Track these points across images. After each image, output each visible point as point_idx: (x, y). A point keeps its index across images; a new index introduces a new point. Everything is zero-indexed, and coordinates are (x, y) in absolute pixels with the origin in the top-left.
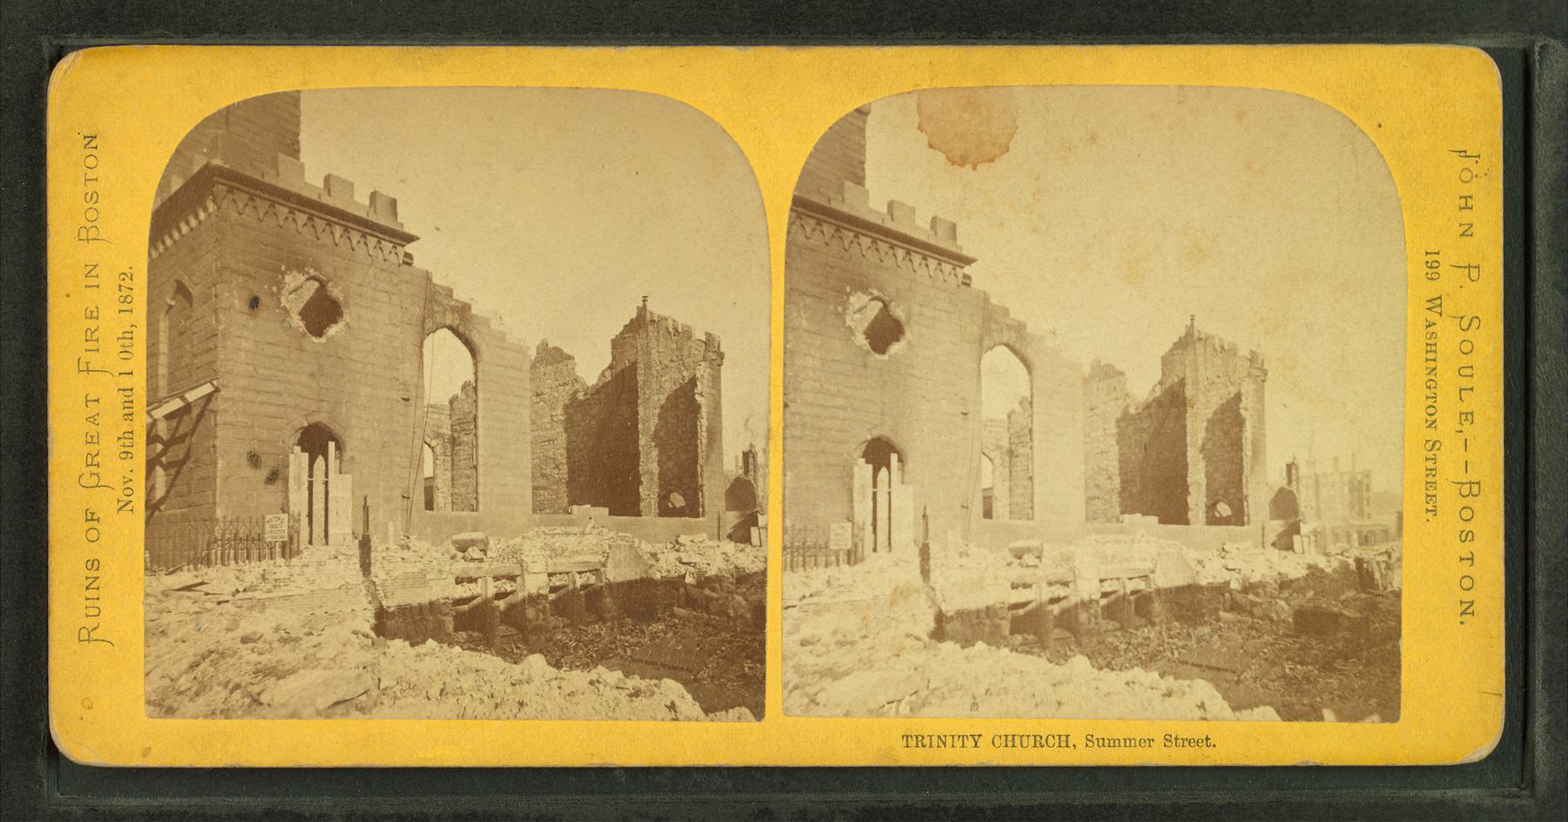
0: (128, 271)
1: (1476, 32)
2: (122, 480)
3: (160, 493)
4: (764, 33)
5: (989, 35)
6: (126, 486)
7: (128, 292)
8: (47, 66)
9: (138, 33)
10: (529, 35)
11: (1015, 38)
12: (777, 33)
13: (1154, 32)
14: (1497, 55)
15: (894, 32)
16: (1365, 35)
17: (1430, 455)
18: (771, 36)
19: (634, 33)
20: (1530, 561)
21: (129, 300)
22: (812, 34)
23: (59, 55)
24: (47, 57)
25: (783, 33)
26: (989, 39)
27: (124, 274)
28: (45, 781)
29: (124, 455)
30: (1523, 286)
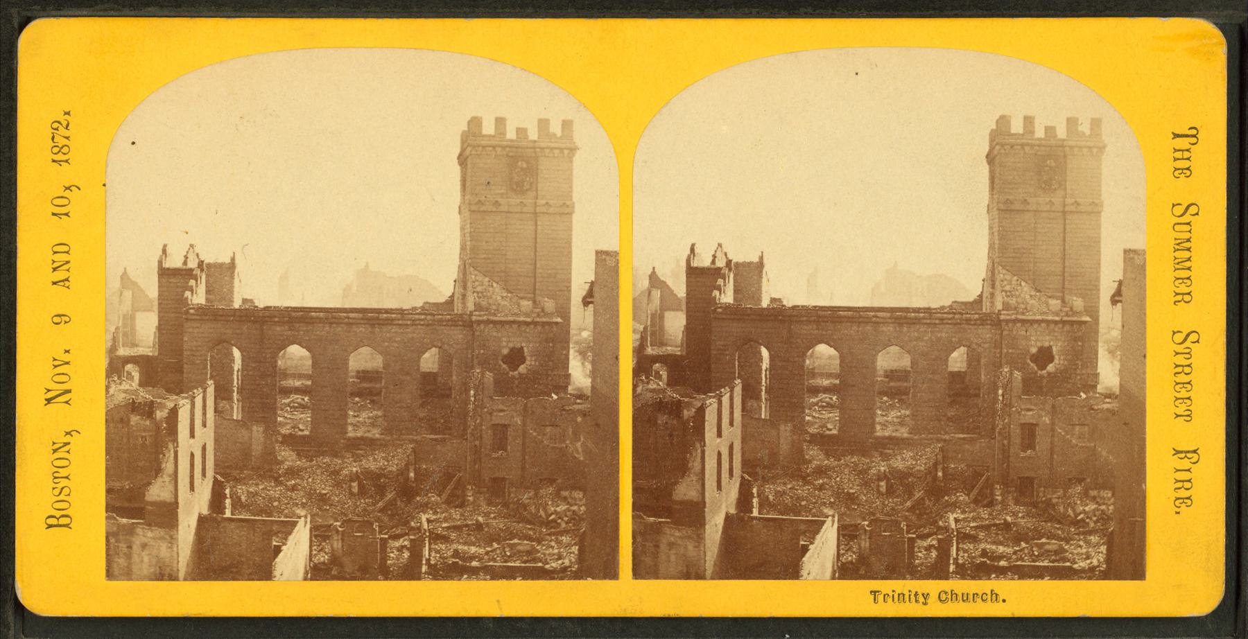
5: (797, 12)
10: (415, 9)
12: (621, 9)
22: (650, 10)
28: (12, 625)
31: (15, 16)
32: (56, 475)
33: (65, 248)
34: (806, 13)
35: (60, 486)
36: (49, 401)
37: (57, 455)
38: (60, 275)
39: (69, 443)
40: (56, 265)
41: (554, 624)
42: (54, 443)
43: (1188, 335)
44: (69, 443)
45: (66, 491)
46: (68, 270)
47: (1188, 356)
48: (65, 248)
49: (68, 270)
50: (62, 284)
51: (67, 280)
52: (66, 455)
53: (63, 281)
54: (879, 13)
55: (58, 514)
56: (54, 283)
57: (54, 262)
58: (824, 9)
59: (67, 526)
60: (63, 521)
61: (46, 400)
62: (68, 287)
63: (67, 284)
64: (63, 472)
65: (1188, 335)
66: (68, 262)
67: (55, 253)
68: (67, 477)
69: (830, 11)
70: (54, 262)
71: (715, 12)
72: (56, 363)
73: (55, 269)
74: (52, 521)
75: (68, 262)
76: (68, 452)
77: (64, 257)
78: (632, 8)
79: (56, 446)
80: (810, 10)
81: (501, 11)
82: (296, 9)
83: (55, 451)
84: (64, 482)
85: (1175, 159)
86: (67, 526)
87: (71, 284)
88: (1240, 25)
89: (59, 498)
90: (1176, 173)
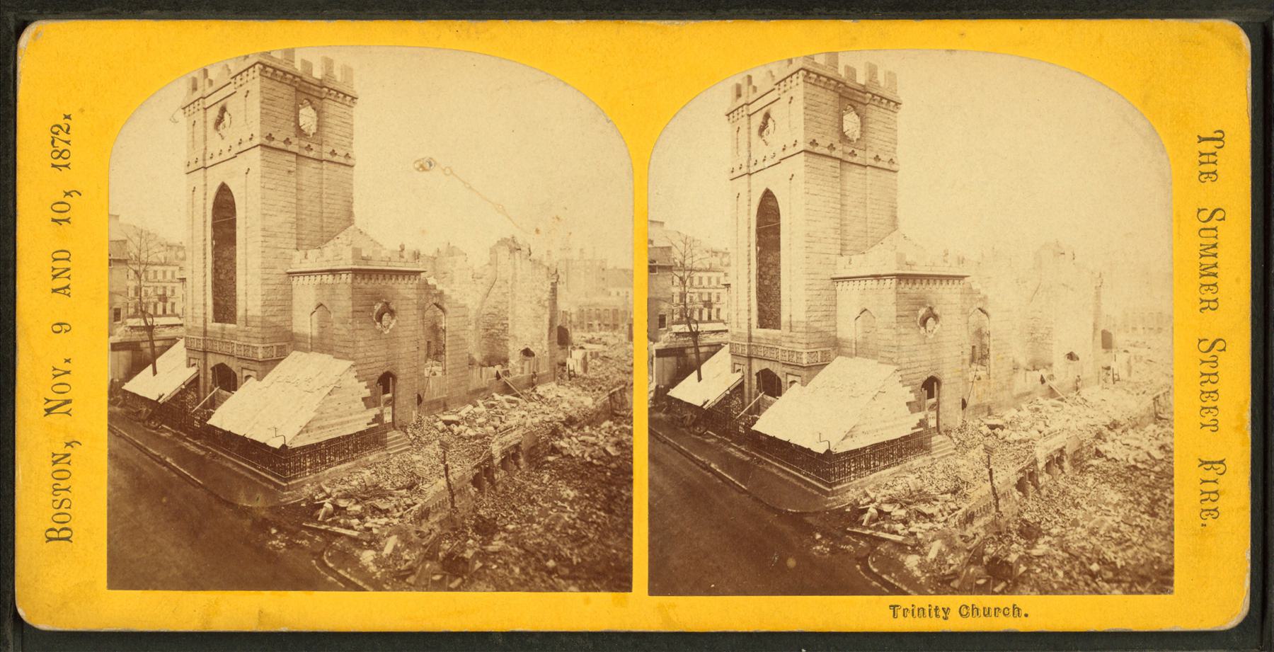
0: (62, 122)
1: (1223, 9)
2: (51, 373)
3: (570, 444)
4: (620, 9)
5: (811, 12)
6: (58, 380)
7: (66, 146)
8: (13, 38)
9: (90, 10)
10: (421, 11)
11: (833, 14)
13: (951, 9)
14: (1246, 28)
15: (731, 8)
16: (1128, 11)
17: (1207, 357)
18: (626, 12)
19: (509, 10)
20: (1262, 445)
21: (65, 154)
24: (13, 29)
25: (636, 10)
26: (812, 14)
27: (60, 127)
29: (57, 328)
30: (1262, 223)
31: (12, 19)
33: (65, 255)
34: (819, 14)
35: (60, 499)
36: (49, 411)
37: (57, 466)
40: (56, 272)
43: (1214, 212)
45: (66, 504)
46: (68, 278)
48: (65, 255)
49: (68, 278)
50: (62, 291)
51: (67, 287)
53: (64, 288)
54: (894, 13)
55: (58, 527)
56: (54, 291)
57: (54, 269)
59: (67, 539)
60: (64, 534)
62: (68, 295)
64: (63, 484)
65: (1214, 212)
66: (68, 269)
67: (55, 260)
68: (67, 490)
69: (845, 11)
70: (54, 269)
71: (727, 13)
72: (56, 373)
73: (55, 277)
74: (53, 534)
75: (68, 269)
76: (69, 463)
77: (65, 264)
78: (642, 9)
79: (56, 458)
80: (824, 10)
82: (298, 11)
83: (55, 463)
84: (64, 494)
85: (1202, 163)
86: (67, 539)
87: (73, 291)
88: (1263, 23)
90: (1202, 178)
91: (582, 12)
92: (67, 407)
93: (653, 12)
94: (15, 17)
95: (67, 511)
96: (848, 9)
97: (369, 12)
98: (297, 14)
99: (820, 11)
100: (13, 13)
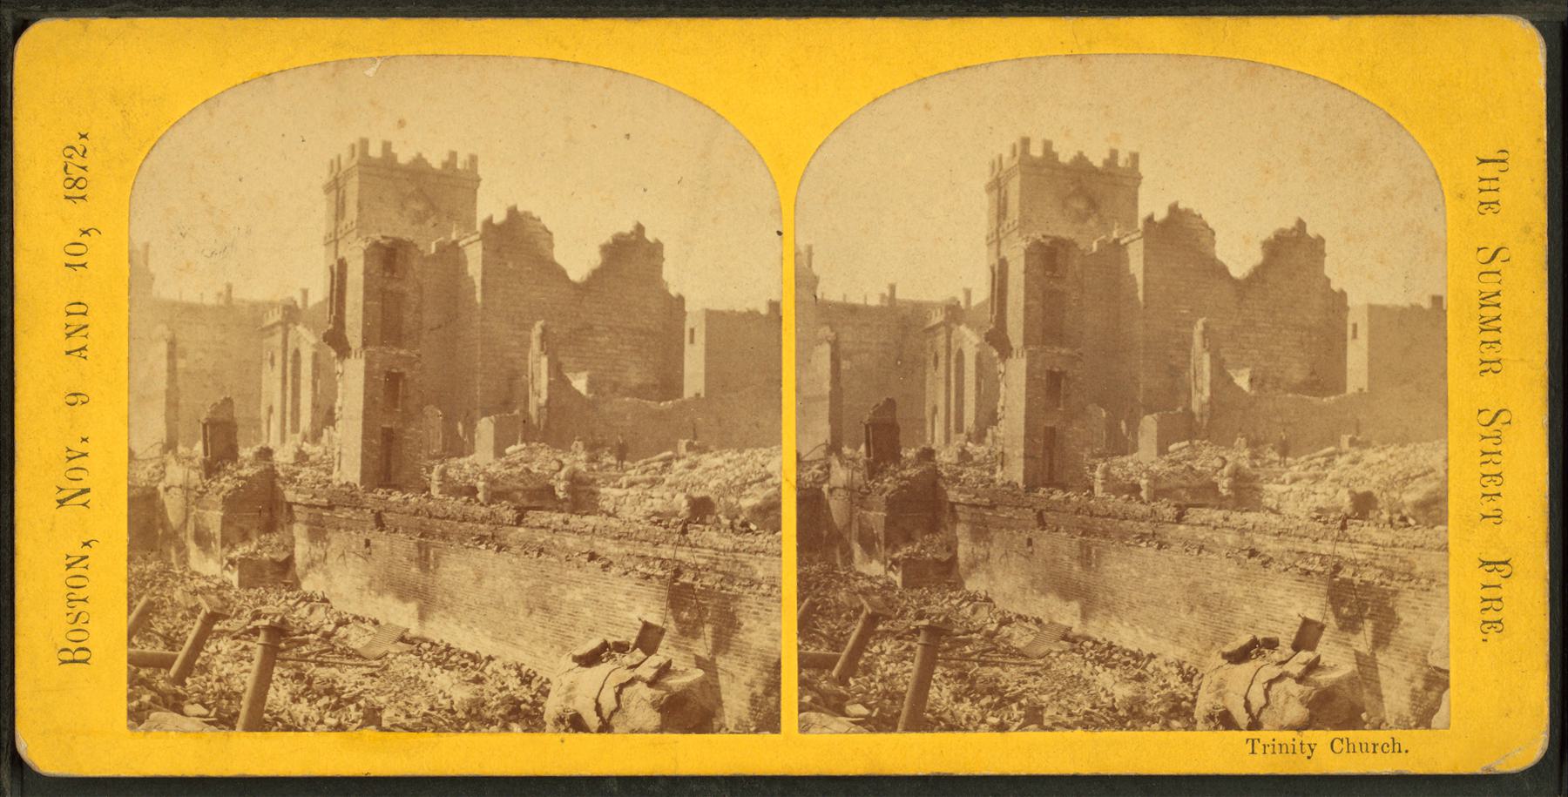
5: (1001, 8)
8: (10, 41)
10: (516, 8)
23: (22, 27)
25: (784, 5)
31: (8, 18)
32: (72, 597)
34: (1012, 10)
36: (61, 502)
38: (76, 342)
39: (87, 557)
41: (695, 787)
42: (68, 557)
44: (87, 557)
45: (83, 618)
47: (1497, 441)
50: (78, 353)
51: (84, 348)
52: (83, 572)
53: (80, 350)
54: (1104, 9)
58: (1036, 5)
59: (85, 661)
60: (81, 655)
61: (58, 501)
63: (84, 353)
64: (80, 594)
69: (1043, 8)
76: (86, 567)
77: (83, 320)
81: (624, 9)
83: (69, 566)
84: (80, 606)
86: (85, 661)
89: (75, 626)
91: (717, 8)
92: (84, 332)
93: (806, 8)
94: (13, 15)
95: (84, 627)
96: (1156, 6)
97: (452, 8)
98: (363, 12)
99: (1012, 7)
100: (10, 11)
